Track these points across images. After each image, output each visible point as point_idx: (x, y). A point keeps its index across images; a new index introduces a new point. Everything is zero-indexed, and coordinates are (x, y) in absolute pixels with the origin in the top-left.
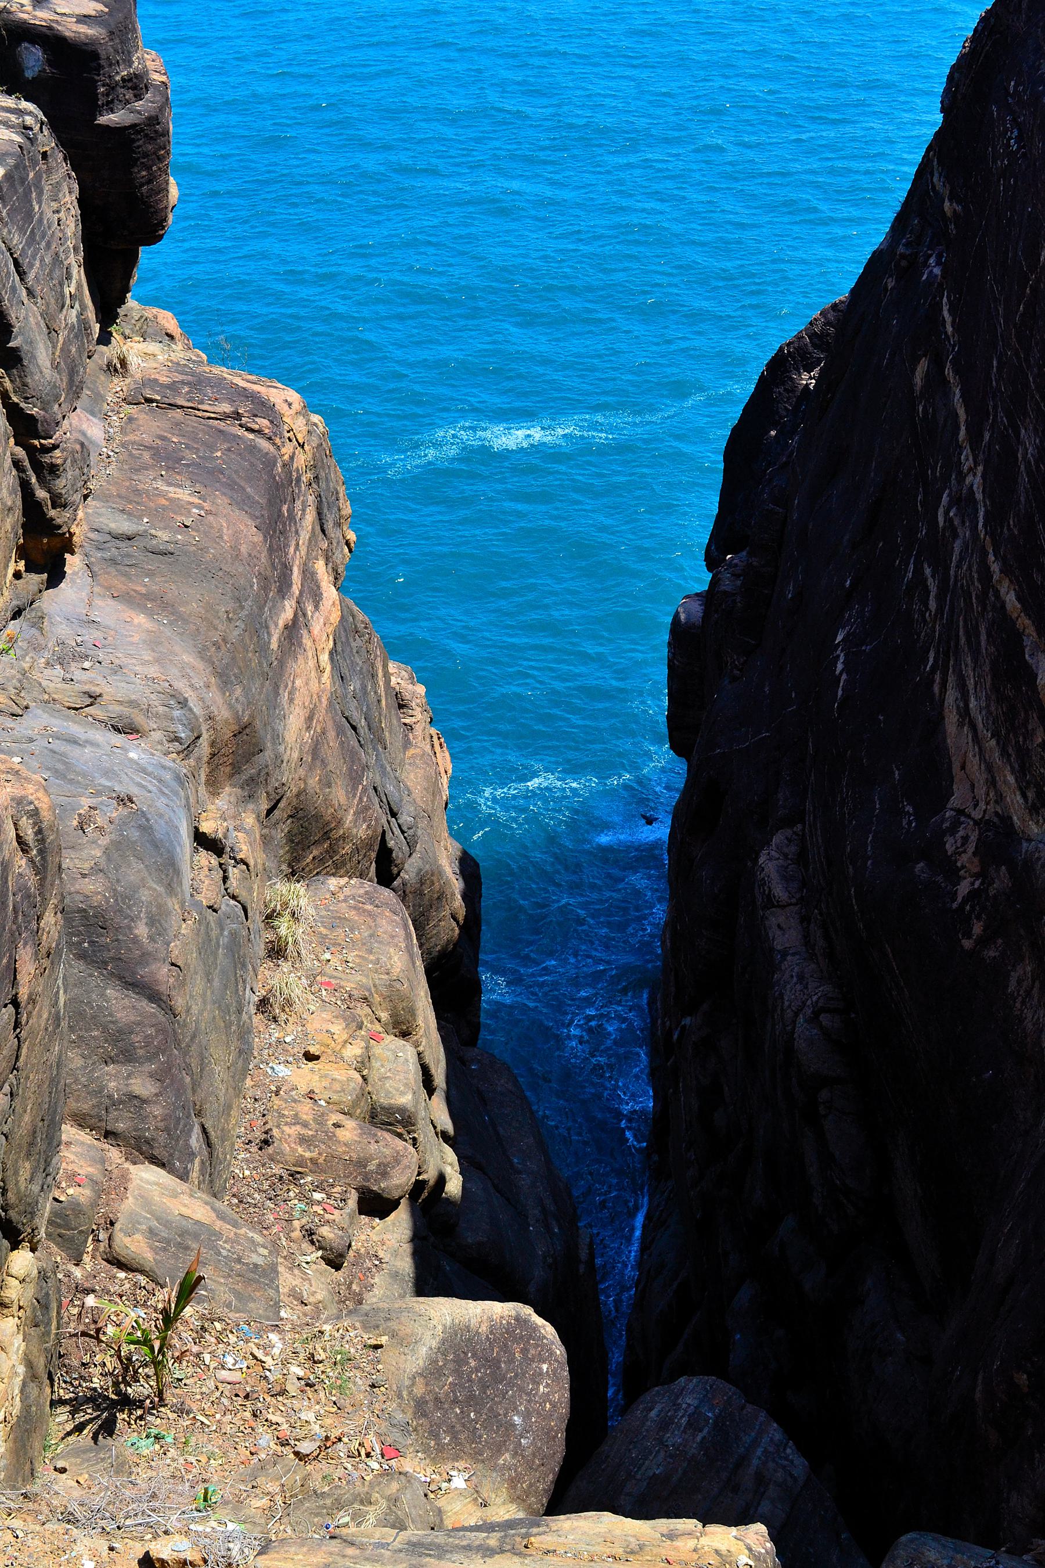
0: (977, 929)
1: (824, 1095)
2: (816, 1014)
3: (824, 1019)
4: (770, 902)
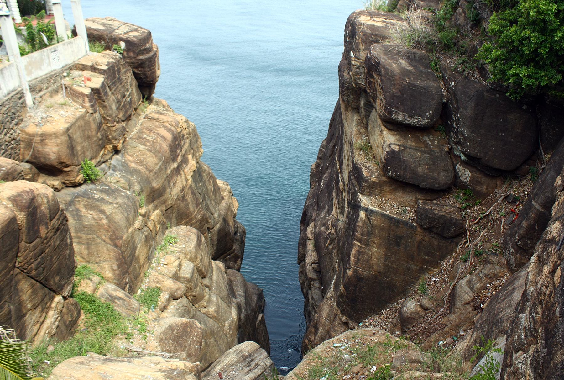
0: (328, 242)
1: (312, 283)
2: (312, 264)
3: (313, 265)
4: (308, 239)
